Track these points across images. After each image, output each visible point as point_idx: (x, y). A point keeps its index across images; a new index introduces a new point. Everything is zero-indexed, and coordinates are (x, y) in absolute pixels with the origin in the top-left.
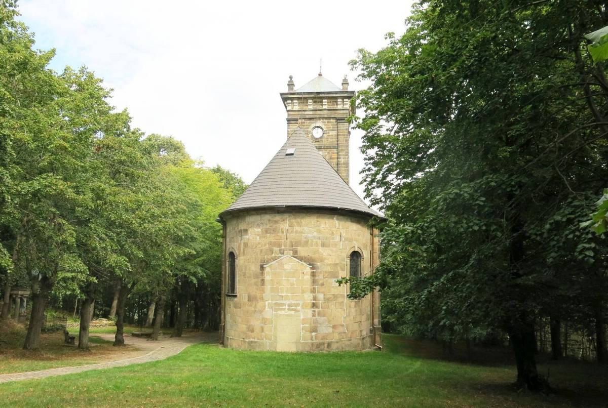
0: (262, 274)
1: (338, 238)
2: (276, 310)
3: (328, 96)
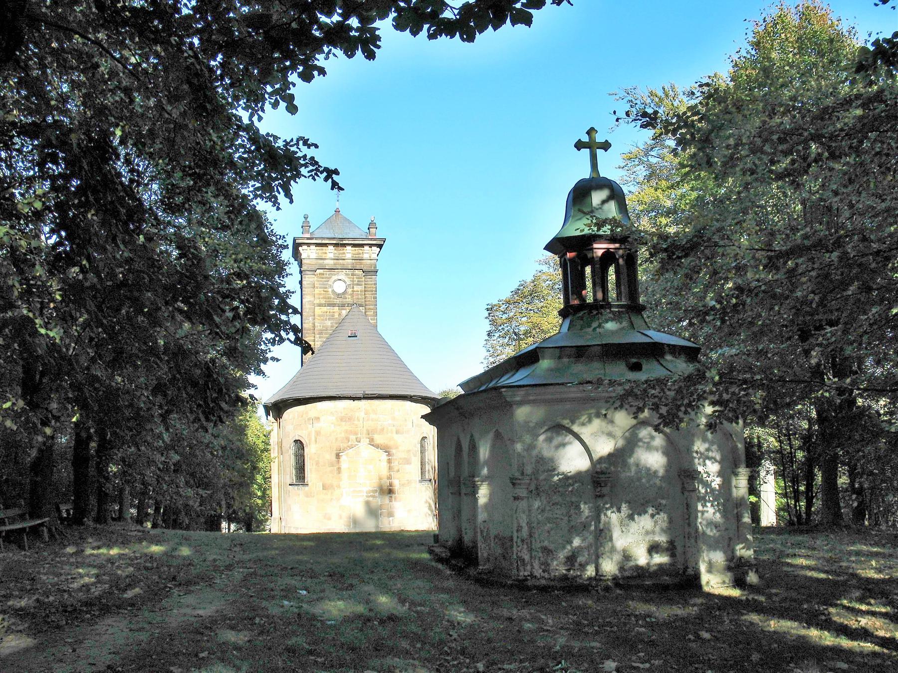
0: (338, 462)
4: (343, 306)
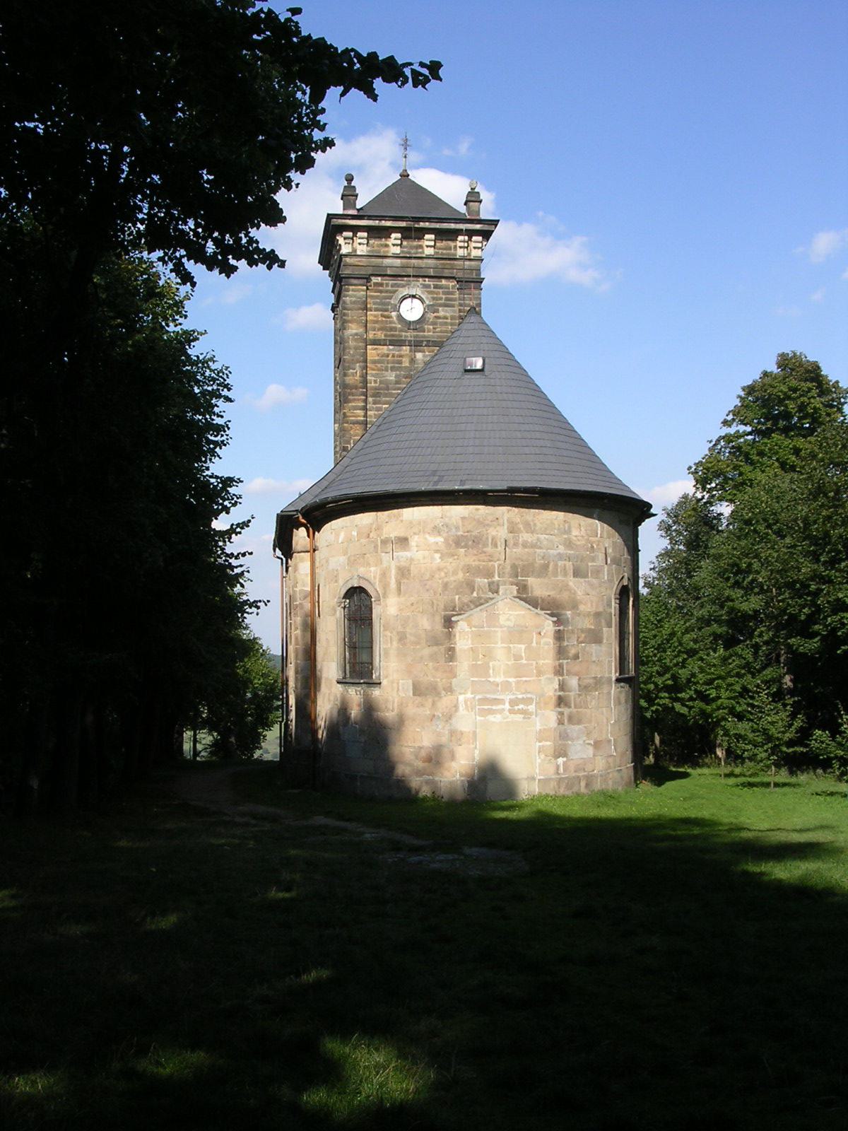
0: (450, 636)
1: (601, 556)
2: (484, 713)
3: (438, 226)
4: (417, 345)
